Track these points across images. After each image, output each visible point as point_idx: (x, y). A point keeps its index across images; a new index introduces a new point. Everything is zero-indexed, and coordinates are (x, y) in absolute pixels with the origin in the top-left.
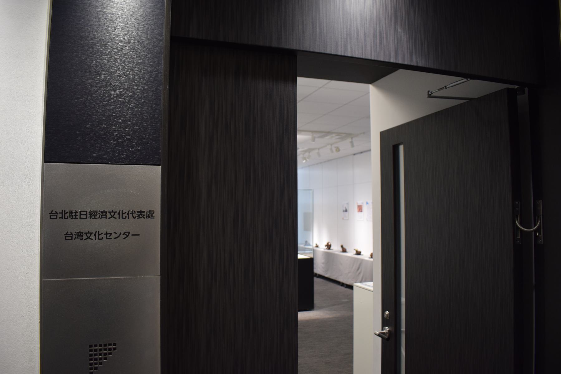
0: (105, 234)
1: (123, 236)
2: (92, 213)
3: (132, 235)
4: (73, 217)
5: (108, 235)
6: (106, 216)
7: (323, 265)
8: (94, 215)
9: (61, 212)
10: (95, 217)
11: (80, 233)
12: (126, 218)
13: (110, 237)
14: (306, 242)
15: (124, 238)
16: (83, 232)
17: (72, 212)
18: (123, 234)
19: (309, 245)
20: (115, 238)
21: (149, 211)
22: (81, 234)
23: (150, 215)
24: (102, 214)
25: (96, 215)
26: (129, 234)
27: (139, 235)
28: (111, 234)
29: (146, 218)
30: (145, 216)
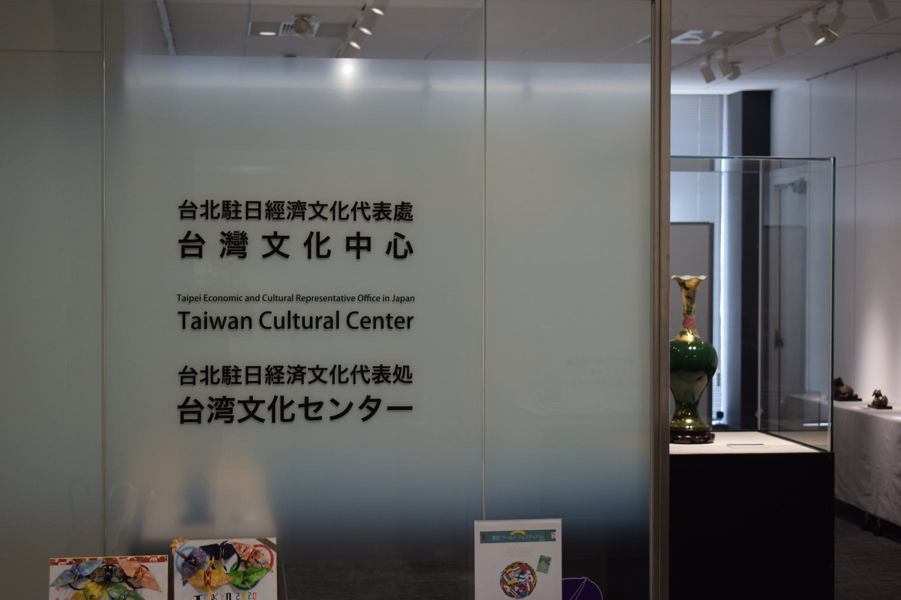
0: (300, 406)
1: (356, 414)
2: (273, 206)
3: (390, 408)
4: (230, 215)
5: (311, 410)
6: (303, 213)
8: (277, 211)
10: (279, 216)
11: (224, 403)
12: (347, 218)
14: (837, 384)
15: (364, 419)
16: (233, 399)
17: (228, 205)
18: (361, 407)
19: (854, 398)
20: (333, 418)
21: (400, 204)
22: (227, 405)
23: (403, 214)
24: (296, 209)
25: (281, 211)
27: (410, 408)
28: (320, 405)
29: (392, 220)
30: (392, 215)
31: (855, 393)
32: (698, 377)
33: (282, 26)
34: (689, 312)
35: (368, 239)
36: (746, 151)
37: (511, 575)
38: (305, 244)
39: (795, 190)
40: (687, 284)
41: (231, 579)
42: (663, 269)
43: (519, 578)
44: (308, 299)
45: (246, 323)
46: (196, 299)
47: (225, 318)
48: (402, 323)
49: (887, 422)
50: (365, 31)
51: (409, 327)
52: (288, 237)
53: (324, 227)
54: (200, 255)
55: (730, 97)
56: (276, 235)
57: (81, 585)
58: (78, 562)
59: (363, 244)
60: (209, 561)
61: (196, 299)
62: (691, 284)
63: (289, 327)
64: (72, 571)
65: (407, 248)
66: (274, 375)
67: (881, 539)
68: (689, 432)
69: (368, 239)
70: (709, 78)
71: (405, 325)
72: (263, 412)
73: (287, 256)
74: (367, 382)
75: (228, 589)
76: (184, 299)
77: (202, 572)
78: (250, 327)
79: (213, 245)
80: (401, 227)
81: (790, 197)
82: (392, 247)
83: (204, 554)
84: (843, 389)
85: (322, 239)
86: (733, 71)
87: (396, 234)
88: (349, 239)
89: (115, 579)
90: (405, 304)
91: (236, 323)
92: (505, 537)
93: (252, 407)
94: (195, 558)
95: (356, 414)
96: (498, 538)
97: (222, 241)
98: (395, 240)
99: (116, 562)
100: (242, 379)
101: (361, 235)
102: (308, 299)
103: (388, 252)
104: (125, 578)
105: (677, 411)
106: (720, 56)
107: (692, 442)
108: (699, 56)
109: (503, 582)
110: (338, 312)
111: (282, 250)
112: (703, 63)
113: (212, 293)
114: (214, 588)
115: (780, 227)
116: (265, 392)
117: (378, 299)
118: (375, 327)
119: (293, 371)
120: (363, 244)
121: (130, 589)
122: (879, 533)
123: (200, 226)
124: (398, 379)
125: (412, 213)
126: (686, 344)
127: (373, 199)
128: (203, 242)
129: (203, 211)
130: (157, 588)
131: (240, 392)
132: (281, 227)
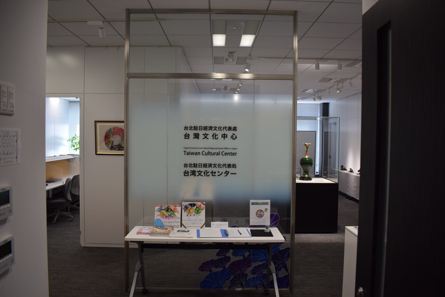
0: (211, 173)
3: (231, 174)
5: (213, 174)
7: (355, 189)
9: (190, 127)
12: (222, 130)
13: (215, 175)
14: (342, 166)
15: (225, 176)
16: (196, 171)
18: (225, 173)
19: (345, 170)
20: (218, 176)
26: (228, 173)
27: (236, 174)
28: (215, 172)
30: (232, 130)
31: (346, 169)
32: (309, 165)
33: (222, 89)
34: (307, 151)
35: (227, 135)
36: (323, 116)
37: (258, 212)
38: (212, 136)
39: (334, 124)
40: (306, 145)
41: (195, 211)
42: (295, 143)
43: (260, 213)
44: (213, 148)
45: (199, 154)
46: (188, 148)
47: (194, 153)
48: (234, 154)
49: (352, 175)
50: (238, 89)
51: (236, 155)
52: (208, 134)
53: (217, 132)
54: (189, 138)
55: (320, 104)
56: (206, 134)
57: (162, 211)
58: (161, 206)
59: (226, 136)
60: (190, 207)
61: (188, 148)
62: (307, 145)
63: (208, 155)
64: (160, 208)
65: (235, 137)
66: (205, 165)
67: (350, 201)
68: (306, 178)
69: (227, 135)
70: (315, 100)
71: (235, 155)
72: (202, 174)
73: (208, 139)
74: (226, 168)
75: (194, 213)
76: (185, 148)
77: (188, 209)
78: (200, 155)
79: (192, 136)
80: (234, 132)
81: (333, 126)
82: (232, 137)
83: (189, 205)
84: (343, 168)
85: (216, 135)
86: (320, 98)
87: (233, 134)
88: (222, 135)
89: (169, 210)
90: (235, 150)
91: (197, 154)
92: (257, 204)
93: (200, 173)
94: (187, 206)
95: (224, 175)
96: (255, 204)
97: (194, 135)
98: (233, 135)
99: (170, 206)
100: (198, 166)
101: (225, 134)
102: (213, 148)
103: (231, 138)
104: (172, 210)
105: (304, 173)
106: (317, 95)
107: (307, 180)
108: (312, 95)
109: (256, 214)
110: (219, 152)
111: (207, 137)
112: (313, 97)
113: (191, 147)
114: (191, 213)
115: (331, 132)
116: (203, 169)
117: (229, 149)
118: (228, 155)
119: (209, 165)
120: (226, 136)
121: (173, 213)
122: (350, 199)
123: (189, 132)
124: (233, 167)
125: (237, 129)
126: (306, 158)
127: (228, 126)
128: (189, 135)
129: (189, 128)
130: (178, 213)
131: (197, 169)
132: (207, 132)
